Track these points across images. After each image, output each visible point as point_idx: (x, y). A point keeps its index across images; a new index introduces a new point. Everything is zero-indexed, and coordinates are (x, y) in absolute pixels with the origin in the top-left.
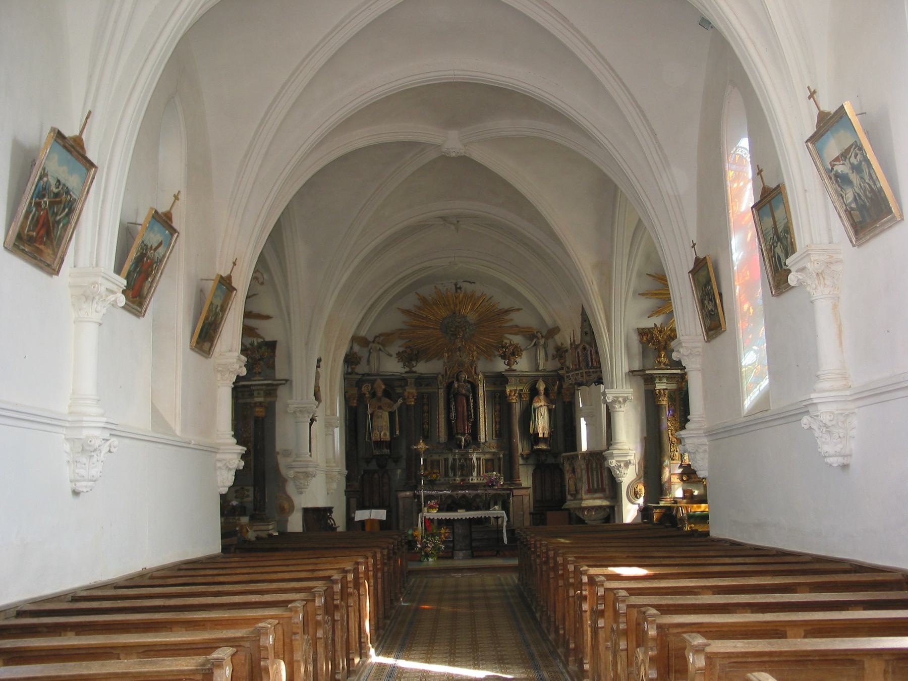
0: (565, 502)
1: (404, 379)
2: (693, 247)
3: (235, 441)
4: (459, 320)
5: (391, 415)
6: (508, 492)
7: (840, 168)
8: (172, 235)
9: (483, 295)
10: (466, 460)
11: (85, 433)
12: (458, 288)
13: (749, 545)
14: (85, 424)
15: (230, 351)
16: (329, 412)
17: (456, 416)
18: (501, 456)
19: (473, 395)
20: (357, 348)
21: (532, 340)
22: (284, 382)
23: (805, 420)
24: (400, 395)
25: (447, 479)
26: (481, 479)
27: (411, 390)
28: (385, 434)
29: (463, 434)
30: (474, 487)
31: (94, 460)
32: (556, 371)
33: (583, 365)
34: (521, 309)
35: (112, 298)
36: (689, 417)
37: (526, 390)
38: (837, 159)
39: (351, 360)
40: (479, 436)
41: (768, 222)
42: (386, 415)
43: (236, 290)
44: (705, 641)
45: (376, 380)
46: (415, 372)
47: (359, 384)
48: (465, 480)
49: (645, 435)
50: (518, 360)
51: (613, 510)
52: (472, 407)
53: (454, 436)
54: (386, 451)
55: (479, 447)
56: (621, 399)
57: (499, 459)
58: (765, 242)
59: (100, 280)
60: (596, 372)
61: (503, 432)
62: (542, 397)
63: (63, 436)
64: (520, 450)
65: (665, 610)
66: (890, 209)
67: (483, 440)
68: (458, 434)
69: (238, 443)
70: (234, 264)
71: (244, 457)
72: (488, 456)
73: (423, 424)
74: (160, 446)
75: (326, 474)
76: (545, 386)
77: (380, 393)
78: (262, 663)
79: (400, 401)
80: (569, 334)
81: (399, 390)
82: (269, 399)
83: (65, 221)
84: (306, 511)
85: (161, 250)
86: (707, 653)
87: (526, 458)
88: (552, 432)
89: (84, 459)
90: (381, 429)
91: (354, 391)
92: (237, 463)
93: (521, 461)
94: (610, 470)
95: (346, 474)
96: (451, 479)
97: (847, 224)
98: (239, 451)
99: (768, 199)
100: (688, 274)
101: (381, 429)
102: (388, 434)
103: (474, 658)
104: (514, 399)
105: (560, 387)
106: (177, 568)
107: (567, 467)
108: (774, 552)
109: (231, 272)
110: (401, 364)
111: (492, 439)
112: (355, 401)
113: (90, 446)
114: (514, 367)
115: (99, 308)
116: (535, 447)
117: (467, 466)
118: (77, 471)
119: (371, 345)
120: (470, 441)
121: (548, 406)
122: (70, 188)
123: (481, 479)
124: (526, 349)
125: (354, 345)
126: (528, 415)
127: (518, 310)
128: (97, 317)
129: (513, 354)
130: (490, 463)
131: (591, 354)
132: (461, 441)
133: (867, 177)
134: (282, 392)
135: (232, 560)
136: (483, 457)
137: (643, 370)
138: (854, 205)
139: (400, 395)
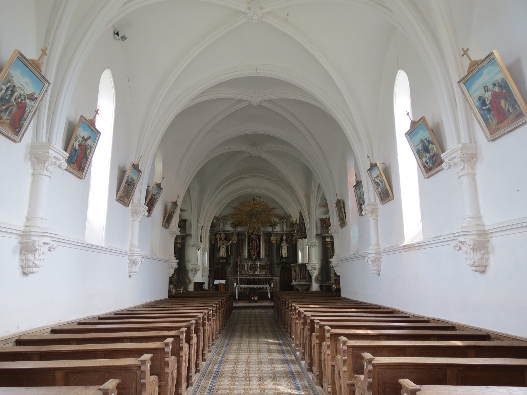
0: (292, 282)
1: (232, 233)
2: (368, 157)
3: (175, 258)
4: (254, 212)
5: (227, 247)
6: (271, 278)
7: (377, 180)
8: (161, 190)
9: (263, 202)
10: (255, 265)
11: (135, 257)
12: (254, 200)
13: (352, 300)
14: (135, 254)
15: (175, 226)
17: (252, 248)
18: (269, 264)
19: (258, 240)
20: (215, 221)
21: (282, 220)
22: (189, 235)
23: (366, 258)
24: (231, 240)
25: (248, 272)
27: (235, 238)
28: (225, 254)
29: (254, 255)
30: (258, 275)
31: (137, 266)
32: (290, 232)
33: (300, 231)
34: (278, 208)
35: (144, 213)
36: (334, 254)
37: (279, 238)
38: (376, 177)
39: (213, 226)
41: (358, 192)
42: (225, 247)
43: (178, 205)
44: (319, 321)
45: (222, 233)
46: (237, 231)
47: (215, 235)
48: (254, 273)
49: (322, 258)
50: (276, 227)
51: (309, 286)
52: (258, 245)
54: (225, 261)
55: (260, 260)
56: (313, 245)
57: (268, 265)
58: (358, 198)
59: (141, 208)
60: (304, 234)
61: (269, 254)
62: (285, 242)
63: (127, 258)
64: (276, 262)
65: (333, 327)
66: (390, 195)
67: (262, 258)
68: (252, 255)
69: (176, 259)
70: (178, 197)
71: (178, 264)
72: (263, 264)
73: (239, 251)
74: (153, 260)
76: (286, 238)
77: (223, 238)
78: (199, 327)
79: (231, 242)
80: (295, 219)
81: (231, 238)
82: (183, 241)
83: (132, 190)
84: (195, 283)
85: (157, 195)
86: (373, 364)
87: (278, 265)
88: (289, 255)
89: (134, 266)
90: (223, 252)
91: (213, 237)
92: (176, 266)
93: (276, 266)
94: (309, 271)
97: (379, 197)
98: (176, 262)
99: (358, 184)
100: (334, 205)
101: (223, 252)
102: (226, 254)
103: (257, 336)
104: (274, 242)
105: (292, 238)
106: (155, 302)
107: (293, 269)
108: (359, 302)
109: (139, 162)
110: (232, 228)
112: (214, 241)
113: (137, 261)
114: (275, 230)
115: (140, 217)
116: (282, 261)
118: (131, 269)
119: (221, 220)
121: (287, 245)
122: (134, 179)
124: (279, 223)
126: (279, 248)
127: (277, 208)
128: (139, 219)
129: (274, 225)
131: (303, 227)
132: (253, 258)
133: (384, 184)
134: (188, 239)
135: (174, 300)
136: (262, 264)
137: (321, 234)
138: (381, 192)
139: (231, 240)
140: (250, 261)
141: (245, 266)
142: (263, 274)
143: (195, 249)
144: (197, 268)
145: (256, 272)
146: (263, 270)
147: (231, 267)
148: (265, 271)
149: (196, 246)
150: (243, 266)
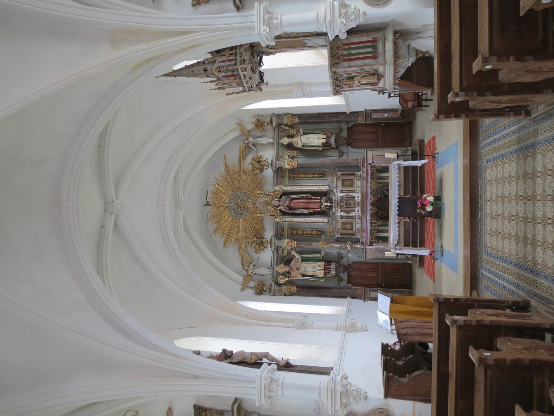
10: (341, 202)
16: (291, 325)
18: (340, 173)
25: (357, 218)
26: (358, 190)
40: (323, 191)
75: (348, 332)
91: (284, 288)
95: (350, 298)
111: (326, 180)
112: (292, 288)
120: (327, 198)
123: (358, 190)
125: (250, 286)
134: (247, 406)
141: (346, 224)
142: (362, 184)
143: (280, 388)
144: (339, 388)
145: (357, 198)
148: (355, 180)
149: (269, 385)
150: (344, 226)
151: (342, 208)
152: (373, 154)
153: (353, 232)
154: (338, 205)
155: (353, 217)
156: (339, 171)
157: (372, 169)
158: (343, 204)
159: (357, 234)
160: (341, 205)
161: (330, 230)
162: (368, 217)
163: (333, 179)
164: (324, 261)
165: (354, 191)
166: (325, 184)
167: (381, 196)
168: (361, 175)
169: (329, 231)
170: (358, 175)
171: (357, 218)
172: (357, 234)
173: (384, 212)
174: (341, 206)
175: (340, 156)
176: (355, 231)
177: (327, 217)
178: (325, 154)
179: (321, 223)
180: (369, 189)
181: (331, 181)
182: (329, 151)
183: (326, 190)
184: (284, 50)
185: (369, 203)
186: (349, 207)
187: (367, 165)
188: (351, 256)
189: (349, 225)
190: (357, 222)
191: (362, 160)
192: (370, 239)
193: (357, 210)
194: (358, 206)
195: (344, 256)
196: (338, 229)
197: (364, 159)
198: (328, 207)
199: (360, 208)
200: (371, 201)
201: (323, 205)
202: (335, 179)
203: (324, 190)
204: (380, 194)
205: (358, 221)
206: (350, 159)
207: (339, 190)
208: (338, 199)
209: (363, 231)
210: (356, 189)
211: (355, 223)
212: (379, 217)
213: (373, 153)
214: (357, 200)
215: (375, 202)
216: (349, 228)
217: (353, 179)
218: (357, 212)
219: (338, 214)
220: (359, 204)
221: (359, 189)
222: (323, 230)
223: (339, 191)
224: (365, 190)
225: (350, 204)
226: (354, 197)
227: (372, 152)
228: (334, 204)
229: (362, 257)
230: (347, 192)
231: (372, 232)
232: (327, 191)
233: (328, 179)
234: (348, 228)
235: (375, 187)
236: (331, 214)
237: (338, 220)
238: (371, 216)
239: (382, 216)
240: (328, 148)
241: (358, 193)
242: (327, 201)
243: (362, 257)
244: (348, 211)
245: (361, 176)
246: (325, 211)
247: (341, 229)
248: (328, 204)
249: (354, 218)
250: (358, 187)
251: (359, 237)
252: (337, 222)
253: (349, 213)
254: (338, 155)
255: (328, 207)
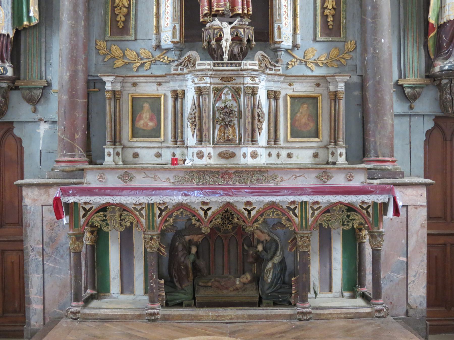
10: (236, 92)
18: (341, 87)
25: (178, 152)
26: (278, 155)
40: (276, 25)
53: (203, 25)
67: (287, 43)
96: (190, 151)
111: (315, 40)
117: (240, 112)
120: (249, 41)
123: (278, 155)
130: (304, 109)
140: (191, 62)
141: (156, 112)
142: (304, 169)
145: (249, 150)
146: (295, 134)
147: (54, 117)
148: (314, 142)
150: (146, 106)
151: (212, 96)
152: (416, 207)
153: (125, 142)
154: (222, 79)
155: (179, 139)
156: (346, 83)
157: (370, 210)
158: (226, 100)
159: (118, 154)
160: (225, 92)
161: (131, 55)
162: (179, 198)
163: (317, 65)
164: (18, 33)
165: (276, 141)
166: (299, 37)
167: (259, 241)
168: (334, 163)
169: (127, 53)
170: (333, 154)
171: (178, 152)
172: (118, 154)
173: (197, 252)
174: (218, 92)
175: (400, 88)
176: (130, 144)
177: (177, 39)
178: (410, 35)
179: (158, 22)
180: (291, 198)
181: (311, 57)
182: (418, 50)
183: (280, 37)
184: (25, 279)
185: (232, 200)
186: (216, 121)
187: (382, 190)
188: (42, 135)
189: (151, 124)
190: (162, 151)
191: (389, 166)
192: (85, 203)
193: (203, 150)
194: (222, 155)
195: (40, 107)
196: (135, 85)
197: (394, 174)
198: (213, 42)
199: (211, 162)
200: (241, 207)
201: (222, 21)
202: (318, 72)
203: (279, 29)
204: (268, 238)
205: (167, 156)
206: (393, 126)
207: (280, 85)
208: (248, 80)
209: (126, 176)
210: (283, 148)
211: (160, 145)
212: (179, 234)
213: (420, 209)
214: (244, 150)
215: (236, 220)
216: (141, 124)
217: (317, 136)
218: (196, 150)
219: (190, 83)
220: (227, 158)
221: (284, 159)
222: (132, 32)
223: (276, 85)
224: (282, 179)
225: (226, 126)
226: (254, 141)
227: (422, 206)
228: (227, 64)
229: (40, 170)
230: (272, 115)
231: (113, 211)
232: (277, 39)
233: (317, 46)
234: (142, 122)
235: (297, 220)
236: (189, 53)
237: (168, 85)
238: (180, 206)
239: (180, 247)
240: (431, 43)
241: (270, 155)
242: (236, 39)
243: (40, 170)
244: (200, 118)
245: (328, 163)
246: (200, 38)
247: (136, 95)
248: (226, 42)
249: (176, 142)
250: (290, 156)
251: (109, 161)
252: (159, 80)
253: (193, 123)
254: (405, 83)
255: (213, 42)
